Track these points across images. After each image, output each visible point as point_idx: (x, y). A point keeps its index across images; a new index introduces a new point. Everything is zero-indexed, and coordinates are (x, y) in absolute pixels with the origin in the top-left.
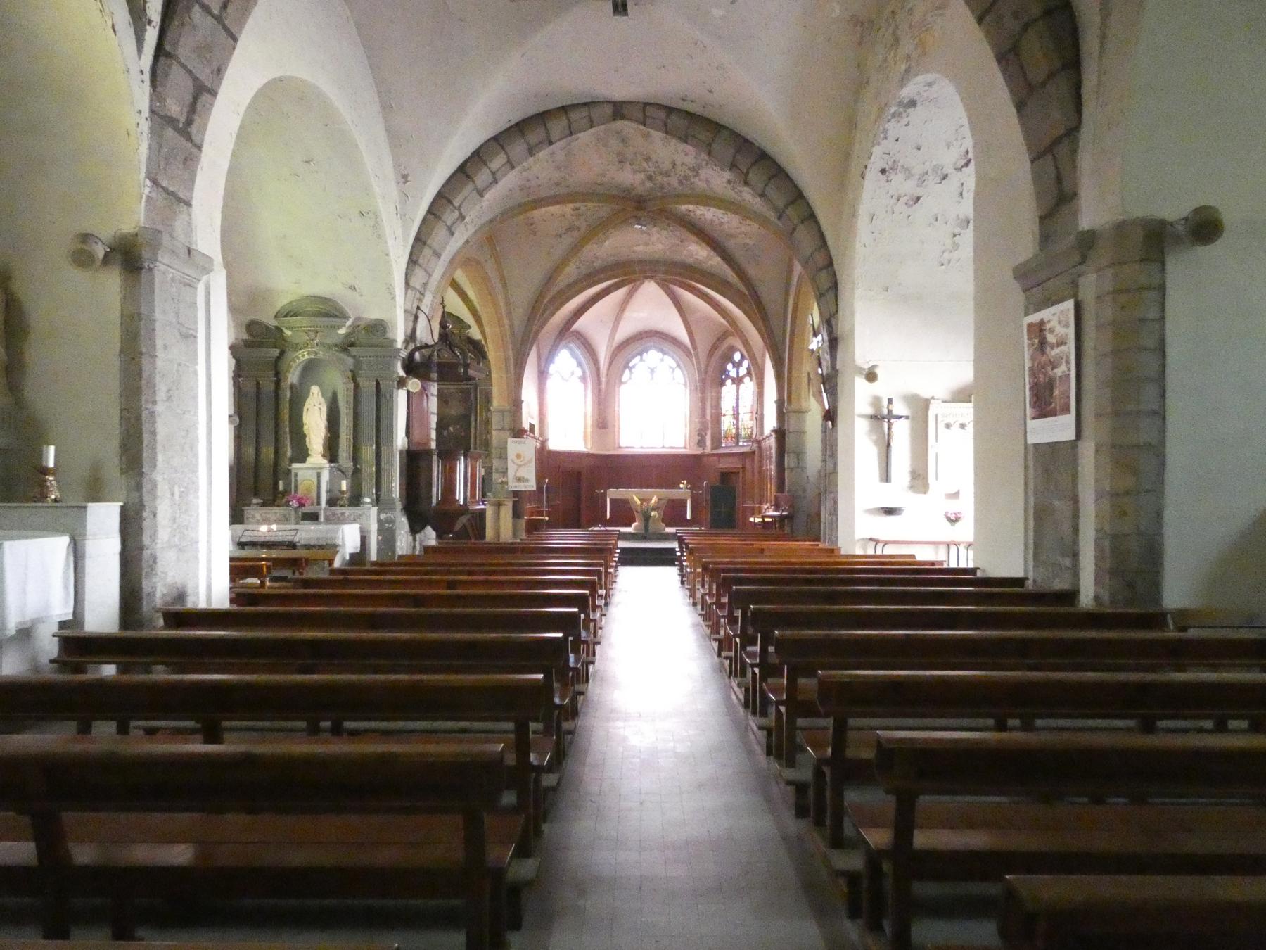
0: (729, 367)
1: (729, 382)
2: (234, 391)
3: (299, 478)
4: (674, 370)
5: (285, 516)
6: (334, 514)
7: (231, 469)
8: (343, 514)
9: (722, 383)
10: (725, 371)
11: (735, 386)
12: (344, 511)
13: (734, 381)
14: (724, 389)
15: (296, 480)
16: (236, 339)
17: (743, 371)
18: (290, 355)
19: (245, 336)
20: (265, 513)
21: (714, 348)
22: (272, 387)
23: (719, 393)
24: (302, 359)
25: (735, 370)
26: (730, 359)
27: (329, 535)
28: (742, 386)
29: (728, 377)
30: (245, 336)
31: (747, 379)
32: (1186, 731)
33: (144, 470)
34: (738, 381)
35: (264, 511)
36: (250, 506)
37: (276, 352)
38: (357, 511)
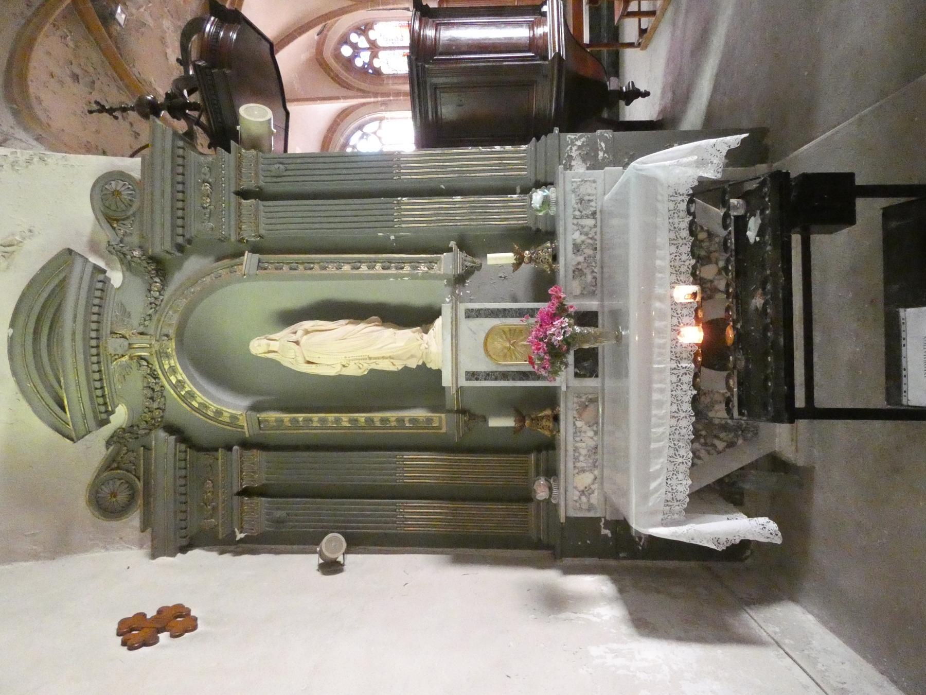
0: (359, 62)
1: (377, 63)
2: (269, 552)
3: (483, 366)
4: (364, 134)
5: (584, 407)
6: (578, 272)
7: (459, 560)
8: (577, 248)
9: (377, 72)
10: (363, 71)
11: (381, 54)
12: (570, 247)
13: (374, 55)
14: (385, 70)
15: (488, 376)
16: (141, 547)
17: (362, 42)
18: (178, 411)
19: (134, 519)
20: (576, 459)
21: (336, 79)
22: (257, 456)
23: (389, 77)
24: (182, 376)
25: (363, 38)
26: (350, 60)
27: (664, 207)
28: (380, 43)
29: (370, 64)
30: (134, 519)
31: (372, 35)
32: (566, 450)
33: (725, 548)
34: (374, 48)
35: (570, 465)
36: (556, 506)
37: (163, 442)
38: (570, 211)
